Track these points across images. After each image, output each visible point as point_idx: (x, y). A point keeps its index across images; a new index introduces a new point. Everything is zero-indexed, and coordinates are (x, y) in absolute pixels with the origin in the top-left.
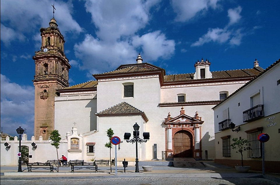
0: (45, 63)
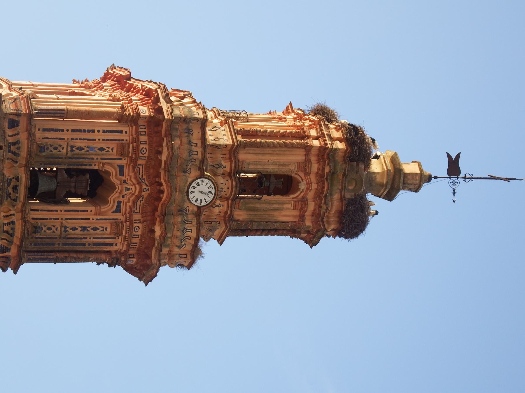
0: (113, 179)
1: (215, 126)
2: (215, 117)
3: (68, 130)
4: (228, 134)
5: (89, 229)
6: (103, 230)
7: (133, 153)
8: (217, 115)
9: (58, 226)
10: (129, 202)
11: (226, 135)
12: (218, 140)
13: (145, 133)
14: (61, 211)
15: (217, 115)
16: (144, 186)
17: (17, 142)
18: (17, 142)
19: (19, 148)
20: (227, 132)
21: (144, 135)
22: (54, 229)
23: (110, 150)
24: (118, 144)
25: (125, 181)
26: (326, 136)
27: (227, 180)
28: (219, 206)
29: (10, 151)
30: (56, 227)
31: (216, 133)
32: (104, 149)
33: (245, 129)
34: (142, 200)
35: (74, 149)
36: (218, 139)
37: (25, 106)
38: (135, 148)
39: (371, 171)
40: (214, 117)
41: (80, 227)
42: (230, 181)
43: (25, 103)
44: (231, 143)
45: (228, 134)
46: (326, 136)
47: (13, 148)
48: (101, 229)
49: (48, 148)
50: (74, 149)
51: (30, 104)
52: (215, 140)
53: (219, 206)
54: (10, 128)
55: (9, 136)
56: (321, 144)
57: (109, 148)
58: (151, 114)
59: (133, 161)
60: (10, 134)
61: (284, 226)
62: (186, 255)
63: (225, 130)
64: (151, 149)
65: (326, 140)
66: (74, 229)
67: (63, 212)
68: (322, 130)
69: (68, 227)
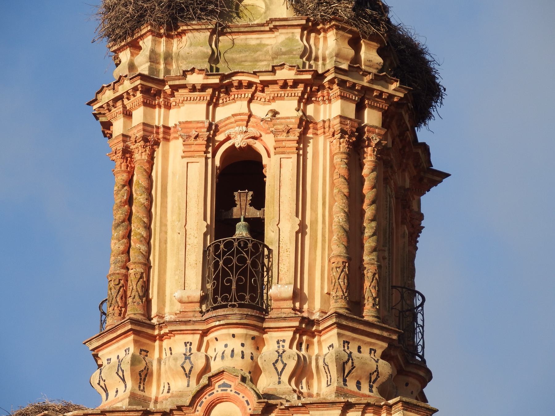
1: (342, 362)
2: (257, 331)
4: (359, 340)
8: (259, 324)
11: (359, 344)
12: (377, 375)
15: (259, 324)
20: (354, 339)
26: (375, 87)
27: (407, 385)
28: (281, 352)
31: (359, 372)
33: (344, 290)
36: (375, 374)
39: (199, 299)
40: (255, 333)
42: (411, 380)
44: (385, 345)
45: (359, 340)
46: (375, 87)
52: (373, 379)
53: (281, 352)
56: (379, 109)
61: (116, 308)
62: (274, 365)
63: (348, 343)
65: (381, 93)
68: (354, 85)
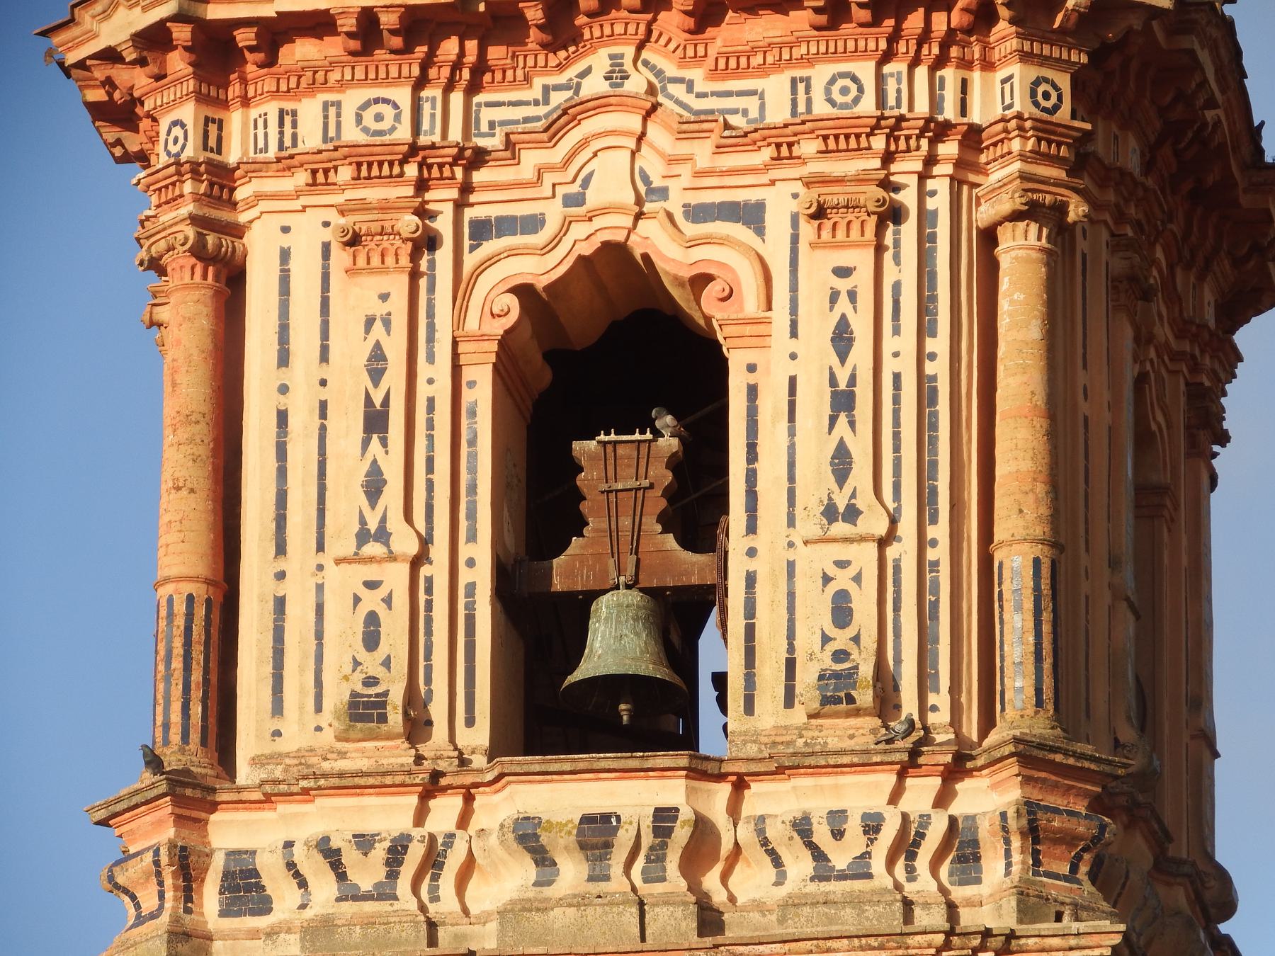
3: (281, 576)
5: (378, 400)
6: (852, 295)
7: (791, 158)
9: (826, 556)
10: (688, 159)
13: (214, 121)
14: (752, 552)
16: (595, 85)
17: (803, 828)
18: (803, 828)
19: (364, 842)
21: (220, 128)
22: (372, 601)
23: (843, 285)
24: (351, 272)
25: (574, 200)
29: (384, 893)
30: (832, 571)
32: (838, 323)
34: (690, 86)
35: (841, 505)
37: (1055, 786)
38: (779, 152)
41: (383, 520)
43: (1044, 780)
47: (367, 874)
48: (843, 305)
49: (370, 681)
50: (373, 526)
51: (1071, 761)
54: (264, 907)
55: (779, 882)
57: (834, 297)
58: (1074, 58)
59: (396, 170)
60: (296, 896)
64: (504, 72)
66: (841, 463)
67: (761, 540)
69: (363, 522)
